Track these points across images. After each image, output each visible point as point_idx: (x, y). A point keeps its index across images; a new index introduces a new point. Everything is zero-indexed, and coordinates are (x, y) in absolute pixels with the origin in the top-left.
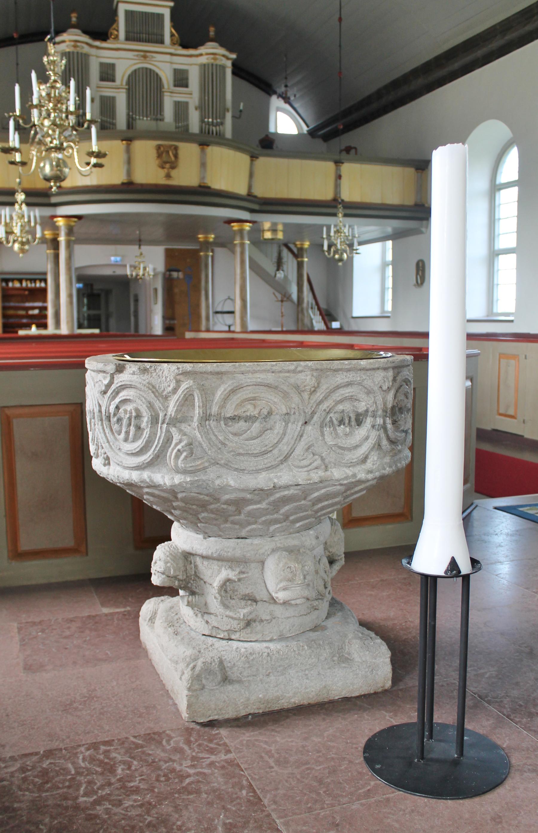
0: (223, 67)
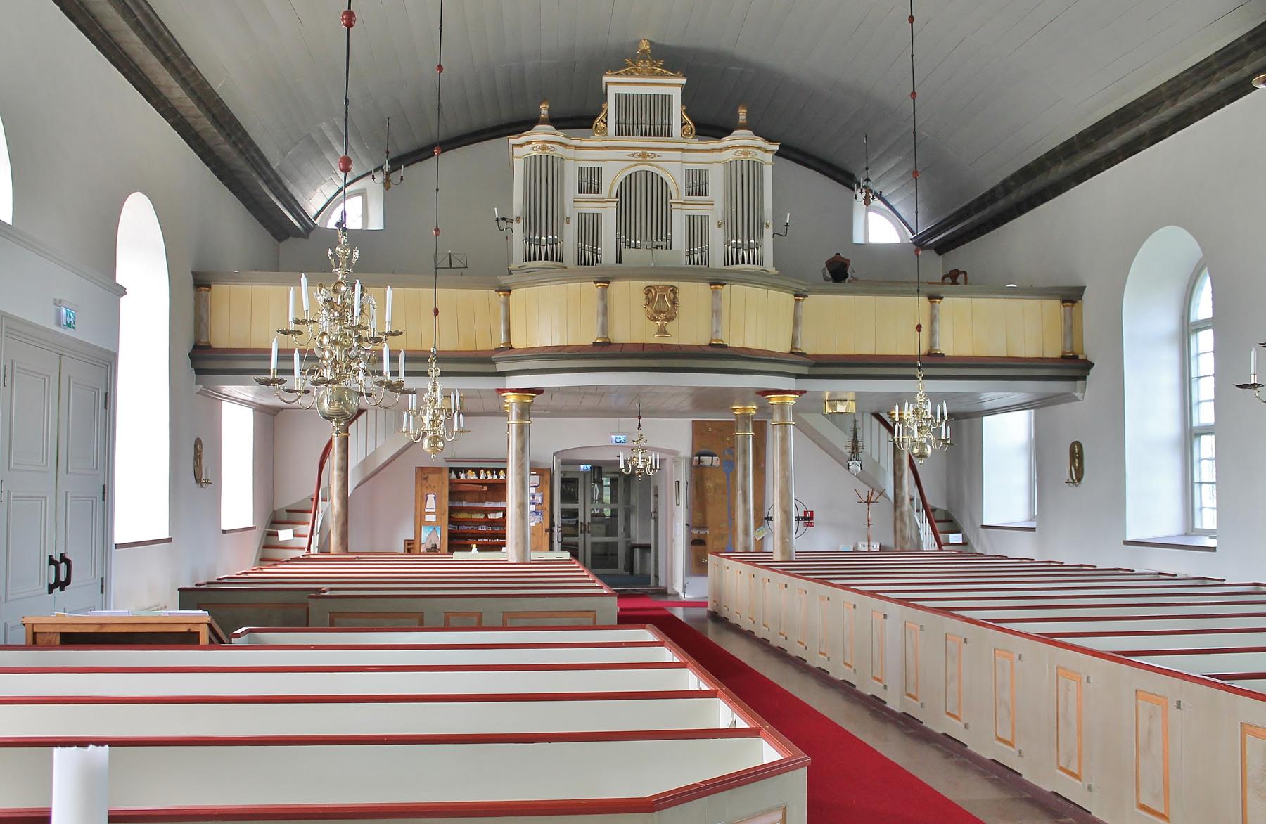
0: (759, 165)
